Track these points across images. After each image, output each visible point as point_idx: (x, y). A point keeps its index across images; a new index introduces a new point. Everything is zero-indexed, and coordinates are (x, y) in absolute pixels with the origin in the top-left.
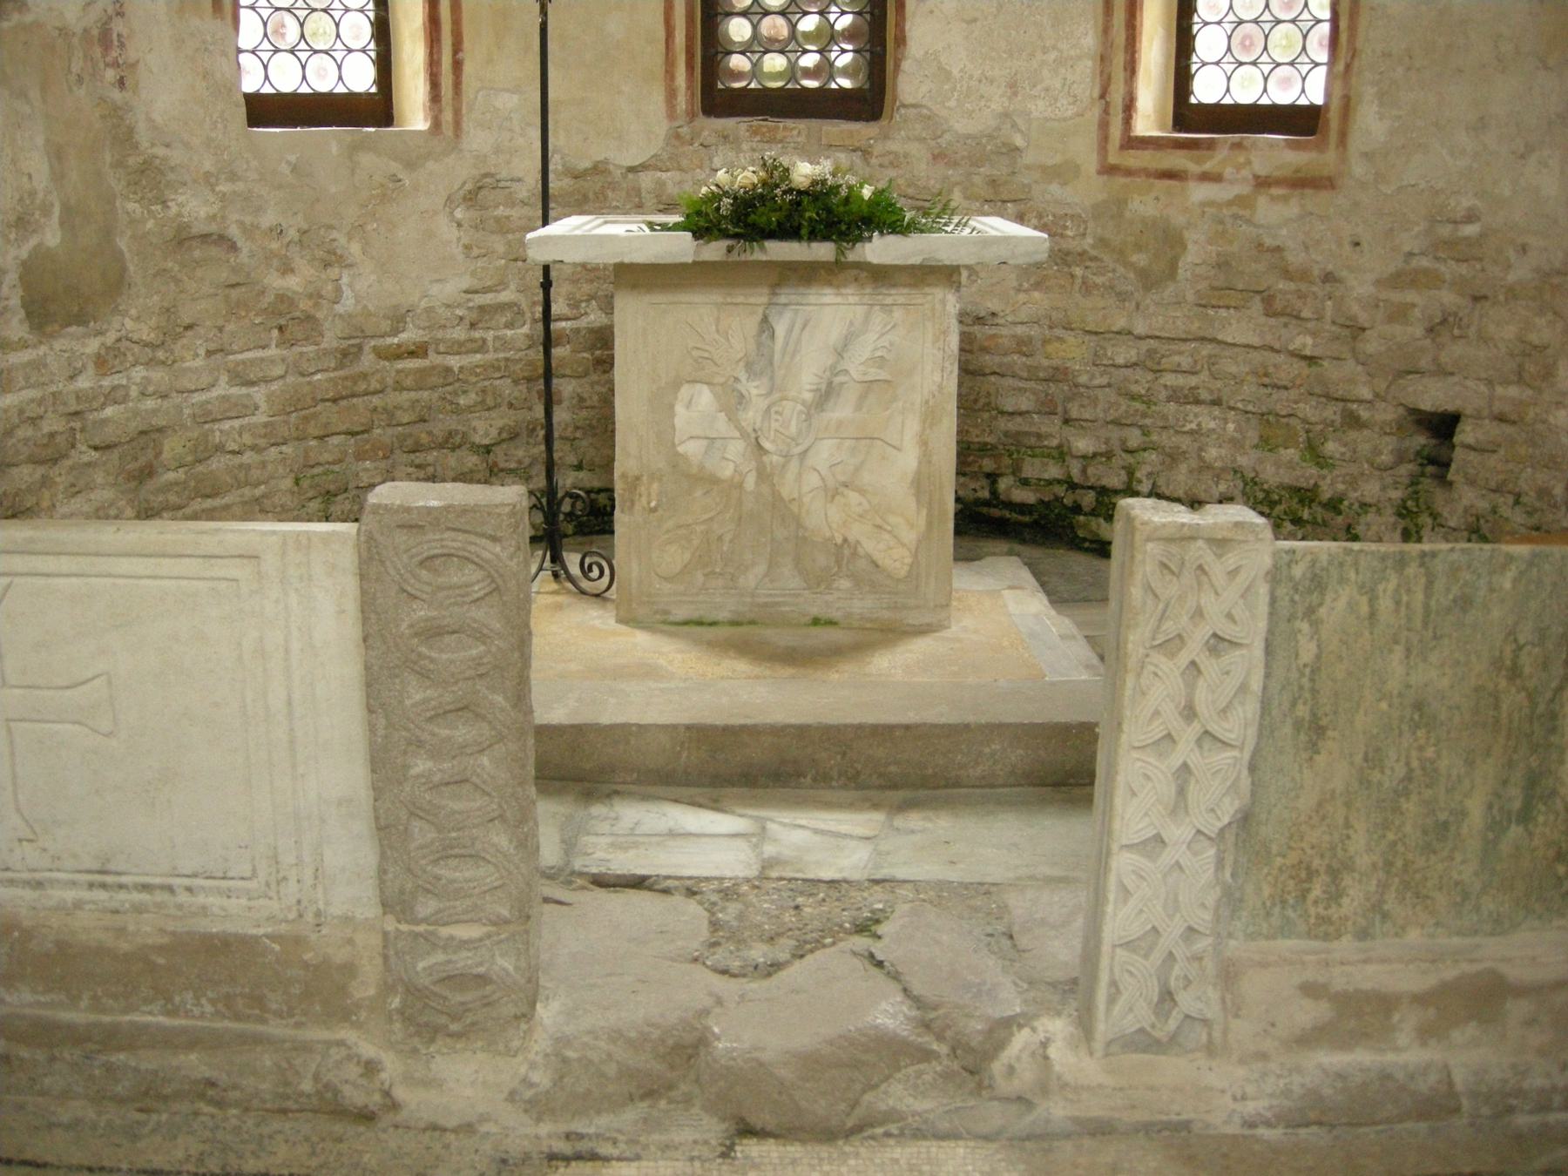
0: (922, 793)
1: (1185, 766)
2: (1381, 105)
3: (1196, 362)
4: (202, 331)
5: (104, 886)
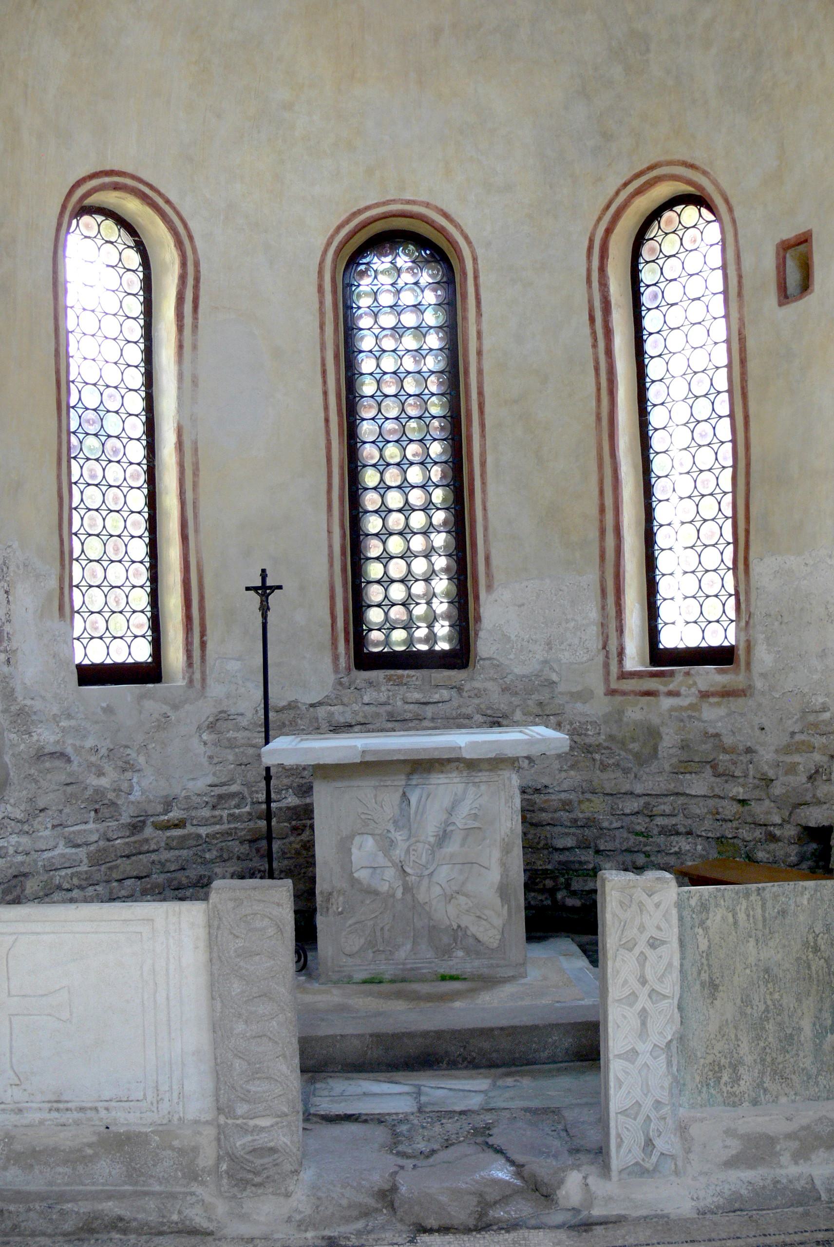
0: (513, 1069)
1: (644, 1010)
2: (768, 645)
3: (674, 809)
4: (50, 812)
5: (58, 1110)
